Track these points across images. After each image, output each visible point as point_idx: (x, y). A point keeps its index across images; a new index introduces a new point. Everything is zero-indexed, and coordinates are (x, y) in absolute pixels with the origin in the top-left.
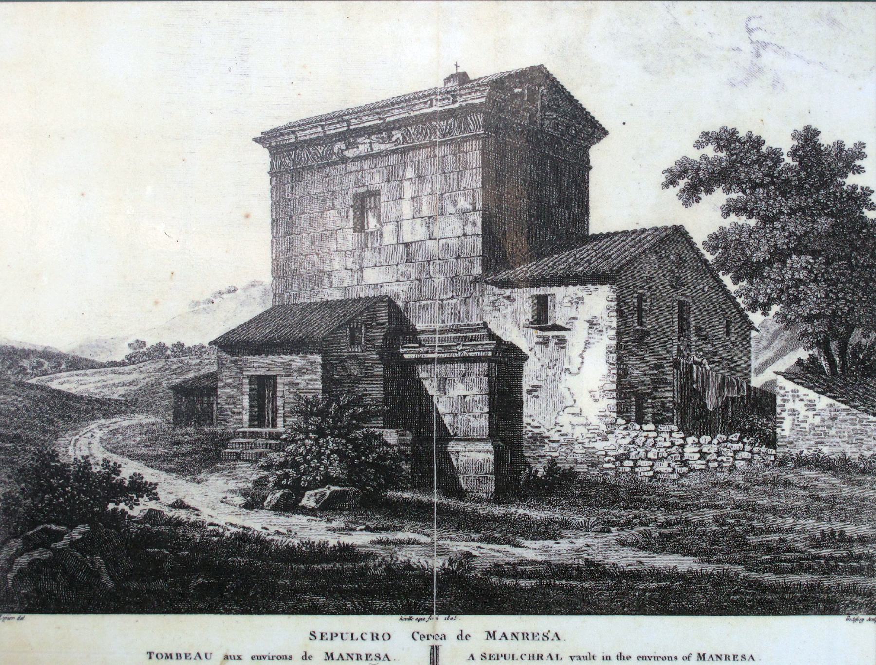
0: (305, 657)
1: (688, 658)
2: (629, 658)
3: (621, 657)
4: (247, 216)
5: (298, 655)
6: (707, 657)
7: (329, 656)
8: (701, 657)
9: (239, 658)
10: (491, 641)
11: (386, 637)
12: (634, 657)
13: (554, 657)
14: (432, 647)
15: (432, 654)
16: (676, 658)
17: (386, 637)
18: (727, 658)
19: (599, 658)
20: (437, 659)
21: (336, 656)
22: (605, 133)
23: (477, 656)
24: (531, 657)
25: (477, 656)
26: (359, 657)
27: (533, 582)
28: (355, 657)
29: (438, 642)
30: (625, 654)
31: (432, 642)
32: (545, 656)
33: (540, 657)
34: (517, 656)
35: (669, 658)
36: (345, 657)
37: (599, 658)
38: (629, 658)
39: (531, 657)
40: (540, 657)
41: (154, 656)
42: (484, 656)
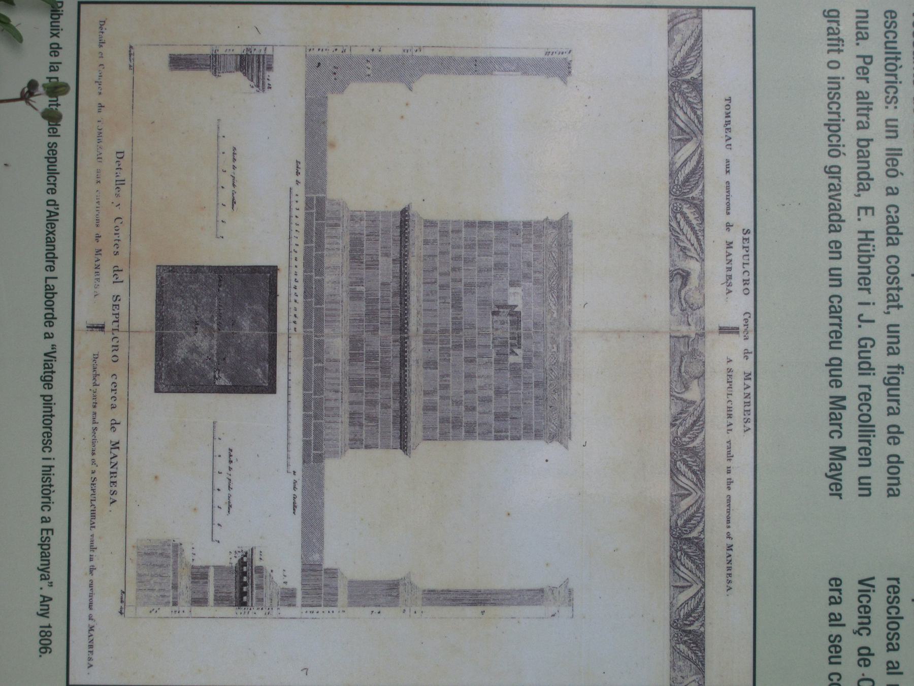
0: (729, 226)
1: (729, 537)
2: (729, 488)
3: (730, 482)
4: (156, 477)
5: (731, 219)
6: (730, 552)
7: (729, 245)
8: (730, 548)
9: (728, 172)
10: (743, 376)
11: (115, 359)
12: (728, 493)
13: (730, 427)
14: (738, 328)
15: (733, 328)
16: (729, 527)
17: (115, 359)
18: (729, 569)
19: (729, 464)
20: (729, 333)
21: (730, 250)
22: (562, 226)
23: (730, 365)
24: (729, 409)
25: (730, 365)
26: (729, 269)
27: (681, 179)
28: (729, 266)
29: (742, 334)
30: (732, 486)
31: (742, 328)
32: (730, 420)
33: (730, 416)
34: (731, 398)
35: (728, 521)
36: (729, 258)
37: (729, 464)
38: (729, 488)
39: (729, 409)
40: (730, 416)
41: (727, 102)
42: (730, 370)
